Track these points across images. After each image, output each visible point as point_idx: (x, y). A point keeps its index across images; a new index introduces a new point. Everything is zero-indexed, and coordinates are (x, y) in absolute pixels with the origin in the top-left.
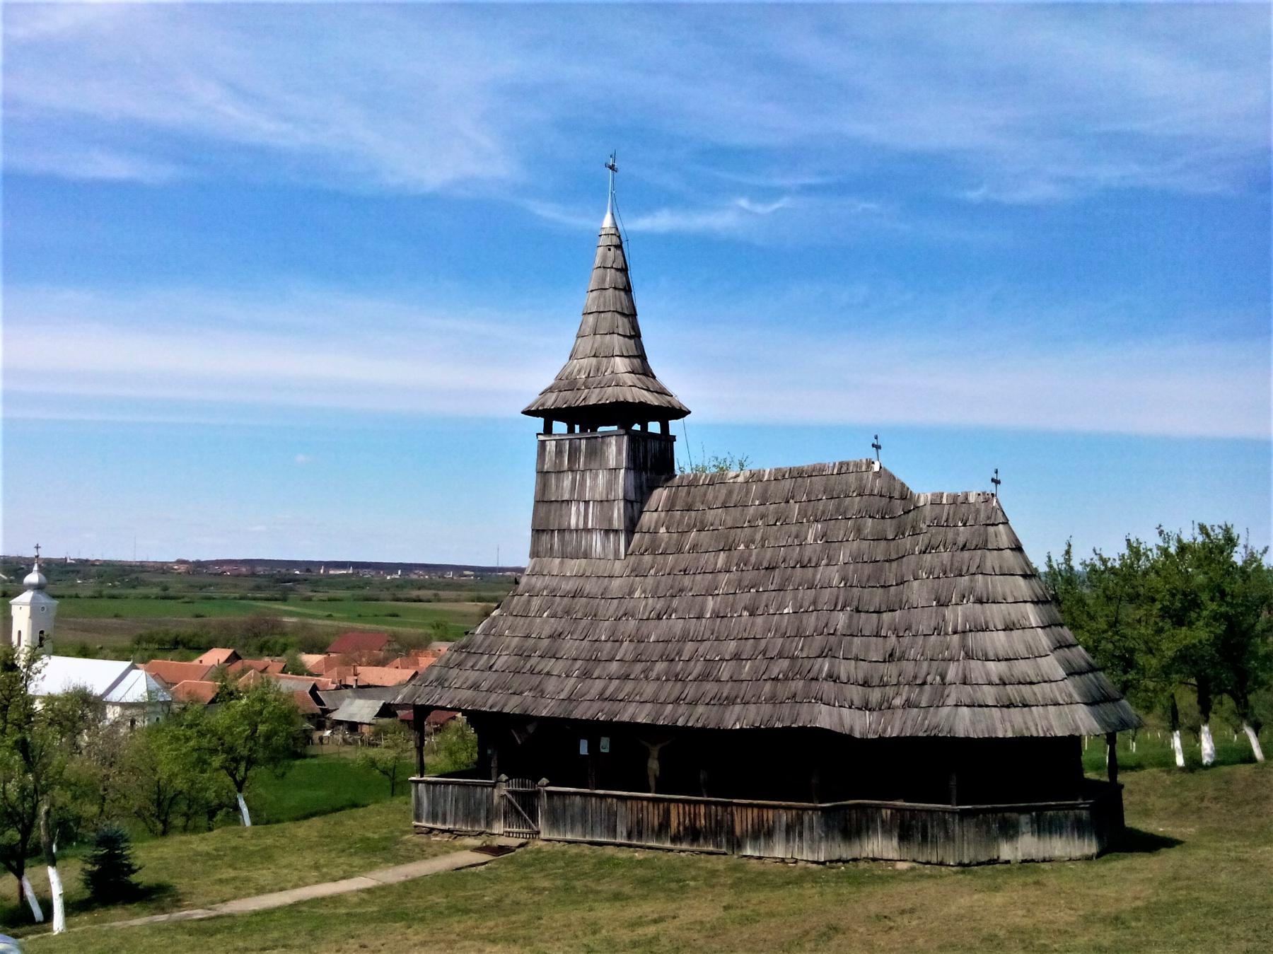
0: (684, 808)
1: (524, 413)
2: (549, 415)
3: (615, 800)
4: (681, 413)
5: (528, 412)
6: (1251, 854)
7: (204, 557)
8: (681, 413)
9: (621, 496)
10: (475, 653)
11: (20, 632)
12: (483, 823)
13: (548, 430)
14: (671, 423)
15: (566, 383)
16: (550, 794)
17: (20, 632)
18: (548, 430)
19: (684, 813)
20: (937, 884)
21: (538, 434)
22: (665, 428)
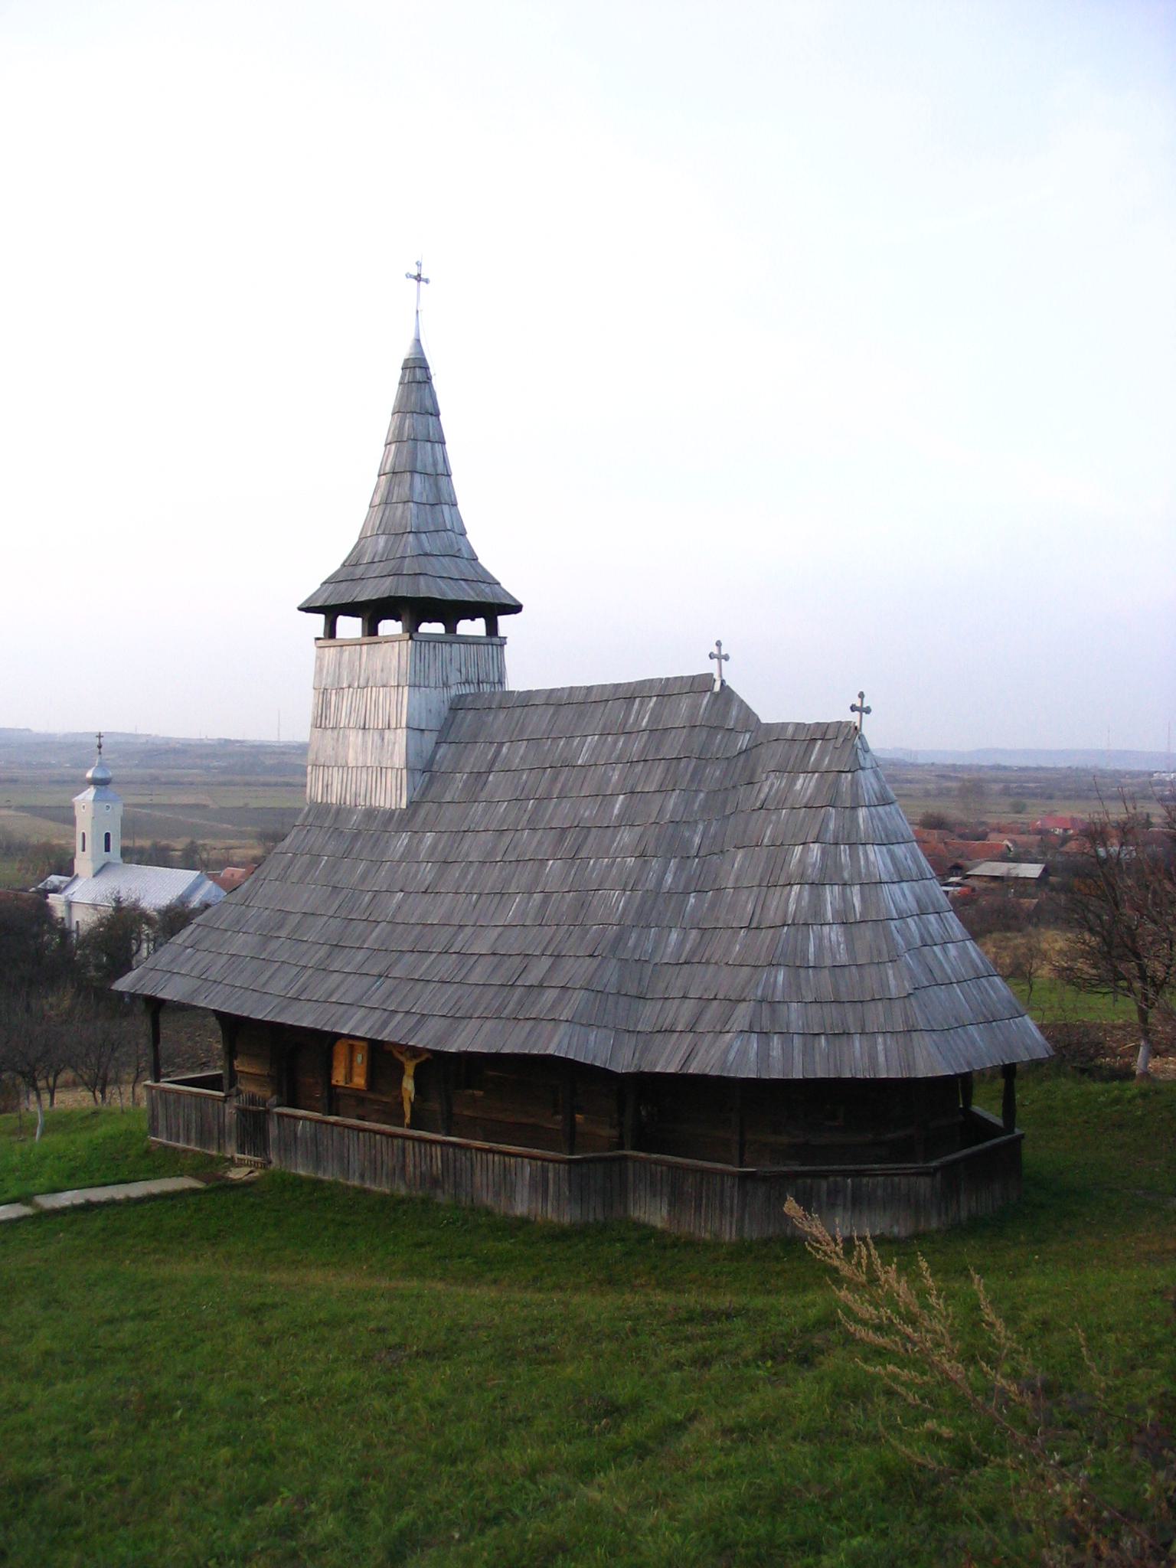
0: (442, 1150)
1: (301, 609)
2: (331, 612)
3: (384, 1138)
4: (516, 608)
5: (307, 609)
6: (218, 1183)
7: (695, 674)
8: (516, 608)
9: (404, 724)
10: (218, 929)
11: (84, 834)
12: (215, 1146)
13: (331, 631)
14: (501, 619)
15: (351, 570)
16: (281, 1115)
17: (84, 834)
18: (331, 631)
19: (425, 1153)
20: (1069, 1343)
21: (318, 639)
22: (492, 629)
